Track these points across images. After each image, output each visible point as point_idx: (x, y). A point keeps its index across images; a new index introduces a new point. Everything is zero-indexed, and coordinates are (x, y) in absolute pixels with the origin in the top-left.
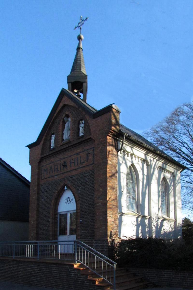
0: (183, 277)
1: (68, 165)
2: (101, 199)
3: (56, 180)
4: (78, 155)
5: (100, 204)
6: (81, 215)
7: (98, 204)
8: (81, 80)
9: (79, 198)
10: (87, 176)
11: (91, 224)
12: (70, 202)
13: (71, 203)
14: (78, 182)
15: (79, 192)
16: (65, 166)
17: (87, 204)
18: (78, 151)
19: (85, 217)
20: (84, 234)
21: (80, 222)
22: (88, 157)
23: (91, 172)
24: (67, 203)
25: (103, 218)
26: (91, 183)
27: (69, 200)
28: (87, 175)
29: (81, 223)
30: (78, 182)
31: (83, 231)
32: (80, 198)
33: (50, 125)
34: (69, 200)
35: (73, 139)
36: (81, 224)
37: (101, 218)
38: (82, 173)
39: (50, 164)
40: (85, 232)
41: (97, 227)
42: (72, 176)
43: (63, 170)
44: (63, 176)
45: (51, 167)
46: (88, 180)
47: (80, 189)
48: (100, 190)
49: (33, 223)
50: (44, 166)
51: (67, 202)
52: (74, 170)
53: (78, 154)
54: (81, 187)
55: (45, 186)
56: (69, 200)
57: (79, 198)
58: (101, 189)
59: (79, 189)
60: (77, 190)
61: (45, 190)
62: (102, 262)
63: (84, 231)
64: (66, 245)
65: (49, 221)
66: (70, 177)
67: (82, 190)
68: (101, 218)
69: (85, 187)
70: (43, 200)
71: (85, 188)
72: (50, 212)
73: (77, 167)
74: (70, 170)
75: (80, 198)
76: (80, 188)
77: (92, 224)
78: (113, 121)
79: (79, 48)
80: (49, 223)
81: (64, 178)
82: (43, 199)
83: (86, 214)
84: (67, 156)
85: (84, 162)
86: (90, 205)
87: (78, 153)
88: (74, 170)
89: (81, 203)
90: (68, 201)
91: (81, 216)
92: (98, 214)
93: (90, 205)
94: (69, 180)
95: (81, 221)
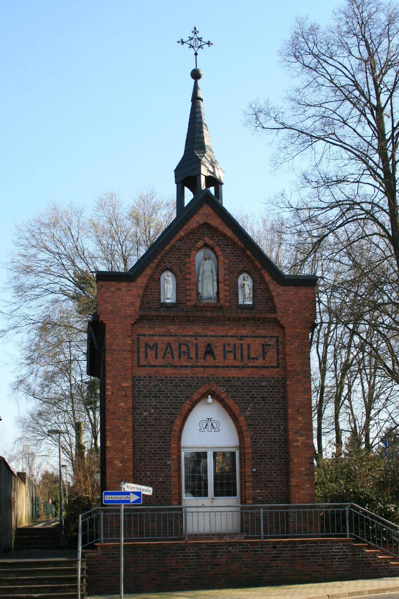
0: (325, 559)
1: (218, 352)
2: (301, 436)
3: (186, 377)
4: (241, 340)
5: (300, 444)
6: (253, 459)
7: (295, 444)
8: (193, 174)
9: (248, 425)
10: (263, 386)
11: (276, 478)
12: (213, 428)
13: (216, 430)
14: (245, 394)
15: (248, 414)
16: (209, 351)
17: (268, 440)
18: (243, 332)
19: (263, 464)
20: (261, 496)
21: (253, 472)
22: (266, 351)
23: (273, 382)
24: (206, 430)
25: (306, 469)
26: (274, 402)
27: (209, 424)
28: (264, 384)
29: (255, 475)
30: (245, 394)
31: (259, 491)
32: (250, 425)
33: (250, 254)
34: (209, 424)
35: (228, 304)
36: (254, 476)
37: (303, 469)
38: (254, 378)
39: (166, 336)
40: (265, 493)
41: (294, 484)
42: (229, 378)
43: (204, 359)
44: (204, 373)
45: (169, 345)
46: (140, 388)
47: (249, 409)
48: (299, 419)
49: (121, 465)
50: (145, 335)
51: (206, 428)
52: (232, 367)
53: (242, 337)
54: (251, 405)
55: (152, 384)
56: (209, 425)
57: (248, 425)
58: (301, 418)
59: (247, 409)
60: (244, 408)
61: (151, 391)
62: (106, 544)
63: (261, 490)
64: (197, 513)
65: (169, 465)
66: (223, 380)
67: (254, 411)
68: (303, 469)
69: (262, 407)
70: (145, 414)
71: (260, 408)
72: (170, 445)
73: (241, 364)
74: (222, 365)
75: (250, 425)
76: (249, 406)
77: (278, 477)
78: (317, 299)
79: (196, 99)
80: (167, 468)
81: (207, 378)
82: (146, 411)
83: (265, 459)
84: (213, 334)
85: (257, 359)
86: (272, 442)
87: (241, 336)
88: (232, 367)
89: (253, 436)
90: (207, 425)
91: (254, 461)
92: (296, 461)
93: (272, 442)
94: (221, 384)
95: (254, 470)
